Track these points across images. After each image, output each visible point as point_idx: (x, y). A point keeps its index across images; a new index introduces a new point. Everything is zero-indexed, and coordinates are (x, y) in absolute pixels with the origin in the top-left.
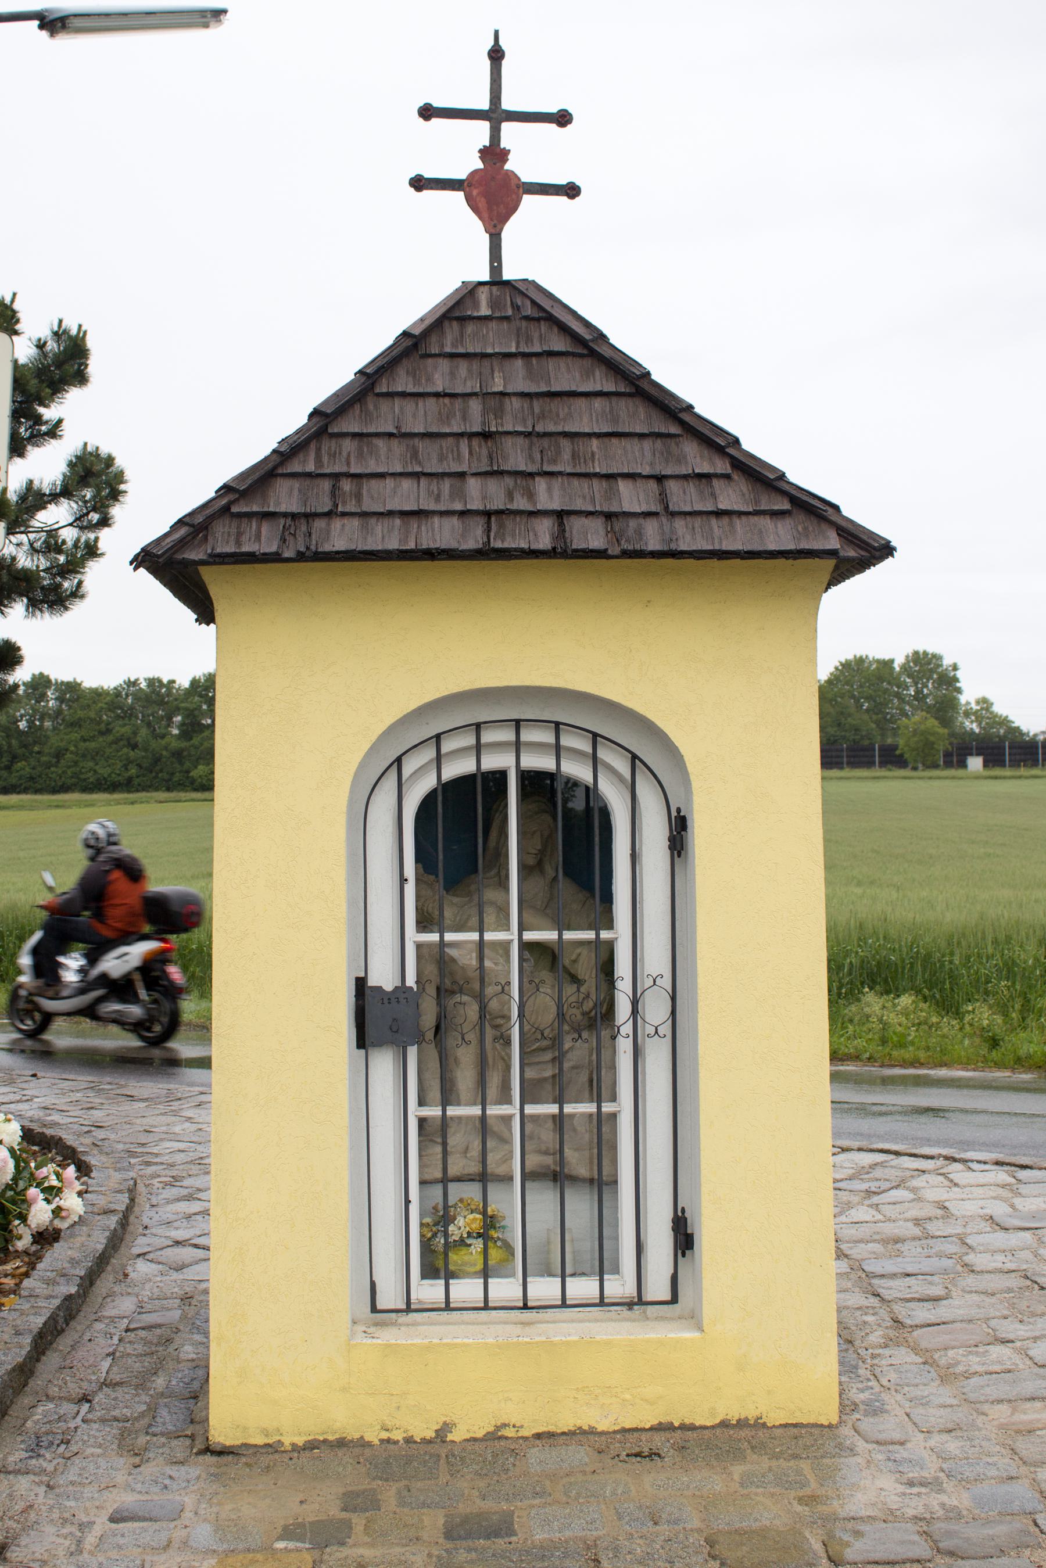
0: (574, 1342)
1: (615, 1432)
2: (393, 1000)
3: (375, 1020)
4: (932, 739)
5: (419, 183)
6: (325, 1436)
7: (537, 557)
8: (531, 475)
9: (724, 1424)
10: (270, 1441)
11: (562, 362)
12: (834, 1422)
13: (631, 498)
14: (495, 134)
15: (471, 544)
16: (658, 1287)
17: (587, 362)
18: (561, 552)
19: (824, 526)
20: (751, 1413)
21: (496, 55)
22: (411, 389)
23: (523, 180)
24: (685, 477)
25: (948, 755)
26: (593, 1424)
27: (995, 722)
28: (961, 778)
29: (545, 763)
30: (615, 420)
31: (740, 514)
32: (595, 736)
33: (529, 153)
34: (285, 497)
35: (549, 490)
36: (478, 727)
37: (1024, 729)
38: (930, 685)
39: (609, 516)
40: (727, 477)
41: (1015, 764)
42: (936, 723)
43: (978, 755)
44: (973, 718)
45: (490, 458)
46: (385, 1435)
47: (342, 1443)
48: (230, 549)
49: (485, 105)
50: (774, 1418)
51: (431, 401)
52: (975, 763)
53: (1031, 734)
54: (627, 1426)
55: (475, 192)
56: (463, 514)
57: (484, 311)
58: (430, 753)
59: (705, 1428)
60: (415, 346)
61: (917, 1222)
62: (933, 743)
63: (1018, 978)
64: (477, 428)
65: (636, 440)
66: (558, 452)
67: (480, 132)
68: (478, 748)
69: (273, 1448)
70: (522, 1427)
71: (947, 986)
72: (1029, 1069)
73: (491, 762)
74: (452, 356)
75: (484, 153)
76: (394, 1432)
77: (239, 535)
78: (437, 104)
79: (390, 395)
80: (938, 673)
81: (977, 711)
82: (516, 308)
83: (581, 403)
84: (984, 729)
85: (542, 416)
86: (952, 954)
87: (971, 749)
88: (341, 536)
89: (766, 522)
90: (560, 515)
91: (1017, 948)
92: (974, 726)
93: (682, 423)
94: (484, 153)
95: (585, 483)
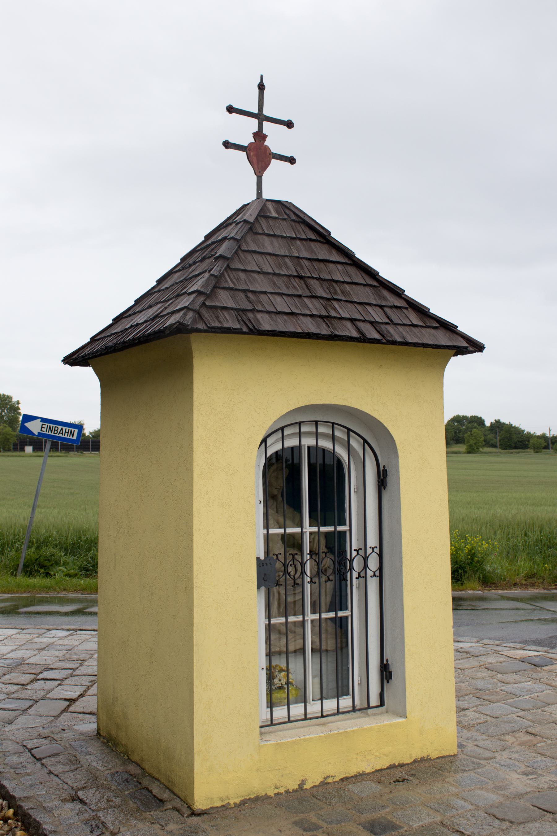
0: (356, 730)
1: (373, 772)
2: (265, 565)
4: (8, 437)
6: (250, 796)
7: (354, 341)
9: (415, 761)
10: (224, 804)
12: (456, 753)
16: (374, 700)
17: (326, 246)
20: (425, 754)
21: (261, 87)
23: (273, 151)
25: (15, 445)
26: (364, 770)
32: (349, 430)
33: (276, 139)
38: (6, 411)
40: (406, 308)
42: (11, 429)
43: (30, 445)
46: (276, 791)
47: (257, 799)
50: (434, 755)
52: (29, 449)
54: (378, 769)
55: (252, 154)
59: (408, 764)
62: (9, 439)
65: (362, 287)
67: (253, 123)
68: (300, 434)
69: (225, 807)
70: (335, 776)
76: (281, 789)
80: (10, 405)
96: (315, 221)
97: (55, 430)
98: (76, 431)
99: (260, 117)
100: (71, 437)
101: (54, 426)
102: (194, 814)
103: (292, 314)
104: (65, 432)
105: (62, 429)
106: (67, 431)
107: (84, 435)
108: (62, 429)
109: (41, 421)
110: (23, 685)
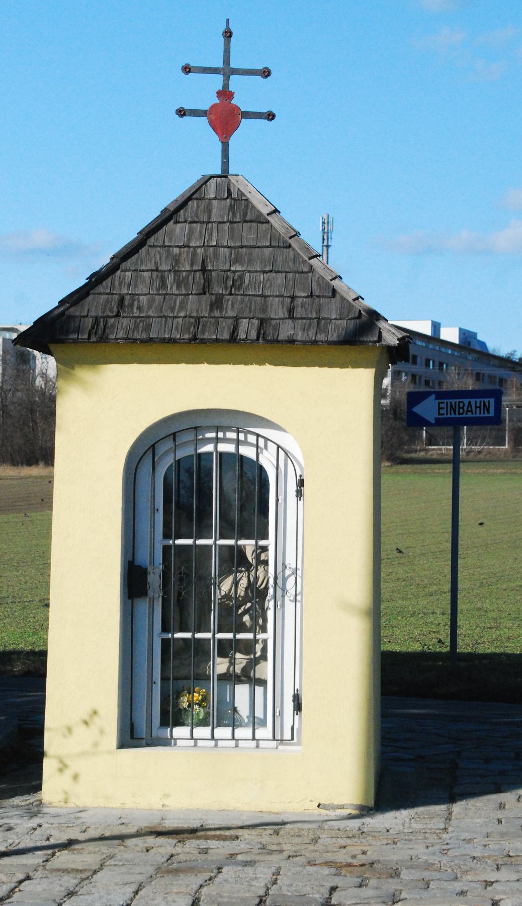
14: (226, 84)
21: (228, 34)
23: (243, 109)
49: (234, 64)
67: (217, 82)
75: (220, 94)
78: (193, 64)
97: (459, 408)
98: (492, 401)
100: (486, 415)
101: (457, 401)
104: (476, 407)
105: (470, 403)
106: (478, 405)
108: (470, 403)
109: (436, 398)
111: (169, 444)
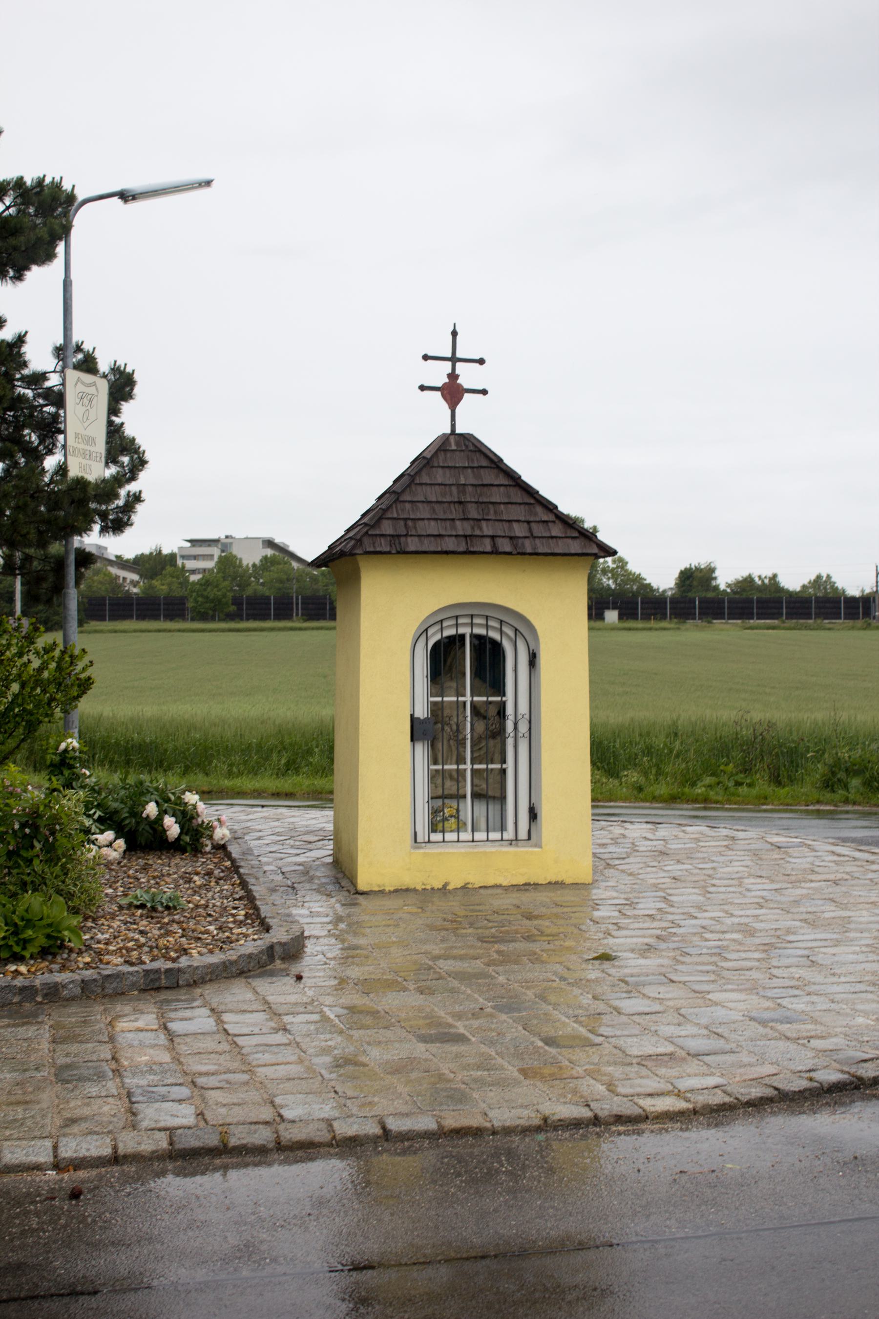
3: (418, 730)
5: (422, 388)
8: (480, 520)
11: (486, 470)
13: (519, 530)
15: (461, 549)
16: (523, 834)
17: (496, 471)
18: (495, 552)
19: (592, 543)
20: (560, 880)
21: (454, 334)
22: (429, 482)
24: (538, 522)
27: (629, 579)
28: (599, 629)
29: (482, 631)
30: (509, 497)
31: (560, 538)
32: (501, 621)
33: (468, 376)
34: (387, 528)
35: (487, 526)
36: (457, 617)
37: (655, 585)
39: (511, 538)
40: (554, 522)
41: (646, 617)
43: (614, 608)
44: (610, 575)
45: (463, 512)
46: (423, 887)
48: (372, 549)
49: (449, 355)
51: (437, 487)
53: (661, 590)
56: (456, 536)
57: (454, 447)
58: (438, 627)
60: (428, 463)
61: (612, 839)
63: (654, 755)
64: (456, 500)
66: (489, 511)
67: (447, 366)
68: (457, 625)
69: (382, 892)
71: (612, 761)
72: (661, 802)
73: (461, 631)
74: (443, 467)
75: (449, 376)
77: (374, 543)
79: (421, 484)
81: (613, 569)
82: (467, 446)
83: (495, 488)
84: (620, 585)
85: (481, 495)
86: (615, 742)
87: (609, 603)
88: (413, 544)
89: (569, 541)
90: (493, 537)
91: (654, 738)
92: (611, 582)
93: (535, 498)
94: (449, 376)
95: (500, 524)
96: (490, 450)
99: (454, 359)
102: (358, 893)
103: (440, 536)
107: (716, 588)
110: (607, 1037)
111: (438, 627)
